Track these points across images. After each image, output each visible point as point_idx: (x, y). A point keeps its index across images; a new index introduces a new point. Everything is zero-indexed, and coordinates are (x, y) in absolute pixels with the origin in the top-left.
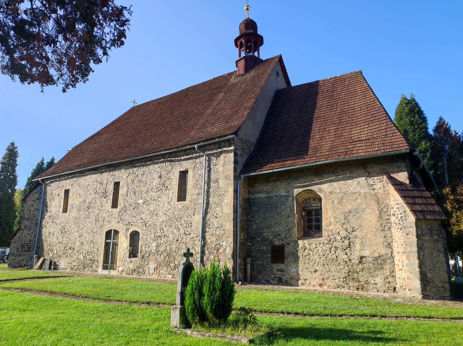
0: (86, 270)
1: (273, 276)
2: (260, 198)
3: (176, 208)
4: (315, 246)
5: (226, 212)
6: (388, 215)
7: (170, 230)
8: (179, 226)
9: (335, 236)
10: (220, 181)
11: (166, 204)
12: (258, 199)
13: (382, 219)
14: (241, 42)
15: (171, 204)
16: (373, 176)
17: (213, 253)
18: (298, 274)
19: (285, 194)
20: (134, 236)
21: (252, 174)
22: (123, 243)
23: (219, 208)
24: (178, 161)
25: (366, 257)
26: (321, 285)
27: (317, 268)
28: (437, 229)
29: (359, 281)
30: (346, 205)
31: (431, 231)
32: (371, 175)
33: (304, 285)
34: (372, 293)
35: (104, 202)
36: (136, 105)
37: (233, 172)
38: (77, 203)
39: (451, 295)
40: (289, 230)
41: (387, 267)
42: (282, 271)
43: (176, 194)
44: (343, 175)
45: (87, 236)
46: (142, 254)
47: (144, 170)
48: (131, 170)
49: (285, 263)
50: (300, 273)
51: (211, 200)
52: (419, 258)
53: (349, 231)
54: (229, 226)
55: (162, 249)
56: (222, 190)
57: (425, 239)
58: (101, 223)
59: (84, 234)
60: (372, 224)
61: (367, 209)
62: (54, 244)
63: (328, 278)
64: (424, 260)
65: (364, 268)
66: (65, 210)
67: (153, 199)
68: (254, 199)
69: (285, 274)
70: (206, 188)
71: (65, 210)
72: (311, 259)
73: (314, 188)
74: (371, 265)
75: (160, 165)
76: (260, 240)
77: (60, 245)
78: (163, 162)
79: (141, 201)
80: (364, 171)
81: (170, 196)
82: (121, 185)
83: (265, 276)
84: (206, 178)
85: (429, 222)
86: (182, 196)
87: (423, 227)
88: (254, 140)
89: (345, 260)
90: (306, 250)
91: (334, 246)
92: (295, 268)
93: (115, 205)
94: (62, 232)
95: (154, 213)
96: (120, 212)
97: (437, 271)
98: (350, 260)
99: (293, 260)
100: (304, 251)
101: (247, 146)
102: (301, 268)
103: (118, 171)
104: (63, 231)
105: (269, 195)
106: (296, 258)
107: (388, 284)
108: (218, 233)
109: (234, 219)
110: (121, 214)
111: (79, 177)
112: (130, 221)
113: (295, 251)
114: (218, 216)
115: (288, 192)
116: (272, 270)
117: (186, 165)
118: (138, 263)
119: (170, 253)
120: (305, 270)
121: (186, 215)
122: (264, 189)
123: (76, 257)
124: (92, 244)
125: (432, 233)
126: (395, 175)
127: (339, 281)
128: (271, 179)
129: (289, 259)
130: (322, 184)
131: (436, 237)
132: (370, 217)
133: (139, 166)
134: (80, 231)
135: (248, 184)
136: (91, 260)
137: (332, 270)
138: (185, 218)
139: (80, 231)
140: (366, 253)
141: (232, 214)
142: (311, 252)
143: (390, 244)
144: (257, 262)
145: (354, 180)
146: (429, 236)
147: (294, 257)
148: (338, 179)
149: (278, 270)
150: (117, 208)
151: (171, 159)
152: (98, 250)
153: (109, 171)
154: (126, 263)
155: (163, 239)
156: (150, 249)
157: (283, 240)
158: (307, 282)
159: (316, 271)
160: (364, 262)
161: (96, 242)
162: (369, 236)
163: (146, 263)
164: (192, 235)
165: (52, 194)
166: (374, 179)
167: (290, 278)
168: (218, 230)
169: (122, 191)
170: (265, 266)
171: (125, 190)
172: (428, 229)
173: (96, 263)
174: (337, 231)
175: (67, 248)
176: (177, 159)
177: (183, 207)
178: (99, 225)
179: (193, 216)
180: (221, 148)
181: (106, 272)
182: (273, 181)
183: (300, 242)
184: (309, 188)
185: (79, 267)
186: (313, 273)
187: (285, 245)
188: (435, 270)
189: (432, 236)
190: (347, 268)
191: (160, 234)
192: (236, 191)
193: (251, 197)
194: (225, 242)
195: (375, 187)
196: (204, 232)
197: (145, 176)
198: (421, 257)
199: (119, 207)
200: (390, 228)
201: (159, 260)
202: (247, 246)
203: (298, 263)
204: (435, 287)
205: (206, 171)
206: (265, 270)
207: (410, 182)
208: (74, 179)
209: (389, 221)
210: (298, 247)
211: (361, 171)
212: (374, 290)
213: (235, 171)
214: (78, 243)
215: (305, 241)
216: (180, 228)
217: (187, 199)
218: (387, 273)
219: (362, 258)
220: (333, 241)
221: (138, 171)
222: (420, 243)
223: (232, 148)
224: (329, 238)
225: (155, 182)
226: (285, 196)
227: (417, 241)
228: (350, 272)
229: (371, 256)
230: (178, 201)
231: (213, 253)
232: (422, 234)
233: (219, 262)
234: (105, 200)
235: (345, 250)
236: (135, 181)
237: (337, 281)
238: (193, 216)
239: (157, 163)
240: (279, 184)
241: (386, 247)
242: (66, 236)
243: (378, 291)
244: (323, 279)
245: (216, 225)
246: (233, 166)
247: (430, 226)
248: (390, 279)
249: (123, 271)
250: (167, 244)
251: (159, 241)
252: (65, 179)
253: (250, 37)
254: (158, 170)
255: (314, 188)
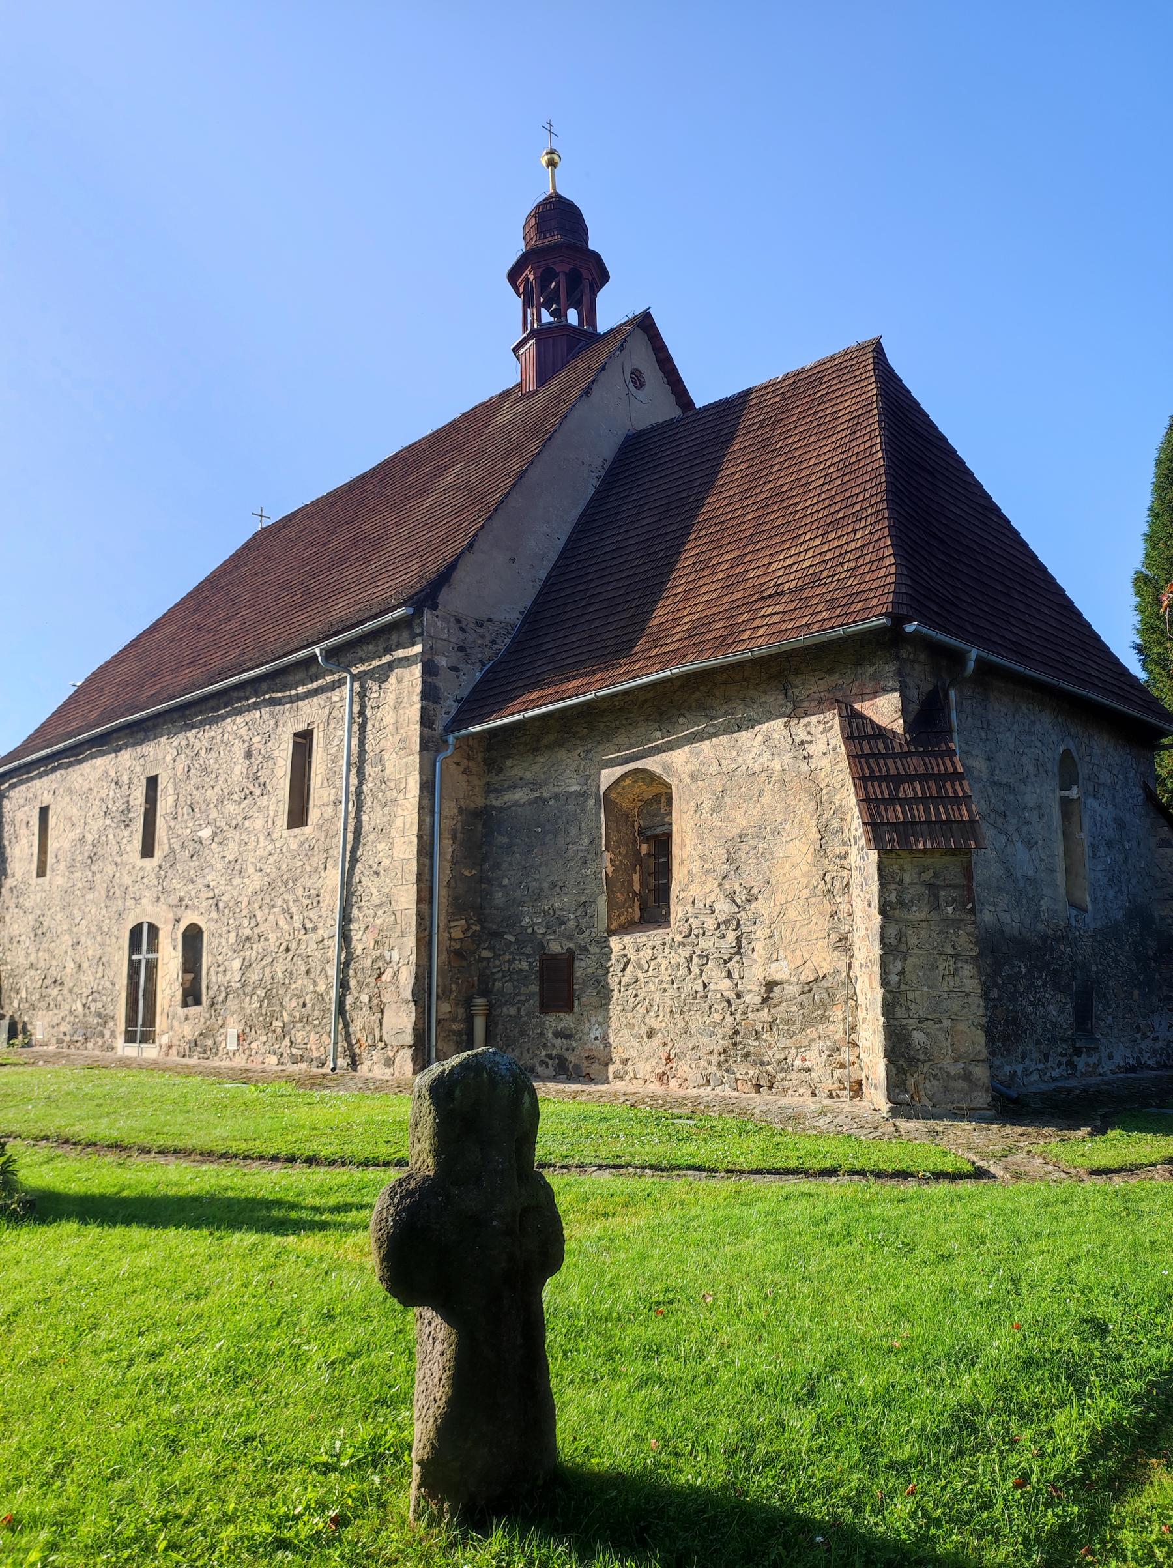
0: (90, 1045)
1: (544, 1053)
2: (516, 804)
3: (284, 850)
4: (650, 952)
5: (402, 856)
6: (845, 844)
7: (271, 917)
8: (291, 904)
9: (702, 918)
10: (386, 757)
11: (262, 839)
12: (509, 807)
13: (826, 856)
14: (527, 279)
15: (274, 836)
16: (806, 714)
17: (368, 985)
18: (607, 1045)
19: (577, 788)
20: (192, 939)
21: (476, 729)
22: (170, 960)
23: (383, 844)
24: (292, 702)
25: (782, 983)
26: (662, 1077)
27: (655, 1024)
28: (957, 881)
29: (762, 1063)
30: (733, 814)
31: (933, 889)
32: (800, 712)
33: (621, 1078)
34: (799, 1100)
35: (125, 841)
36: (267, 523)
37: (418, 727)
38: (67, 845)
39: (992, 1105)
40: (586, 905)
41: (837, 1013)
42: (566, 1035)
43: (284, 808)
44: (726, 713)
45: (89, 943)
46: (211, 993)
47: (213, 734)
48: (180, 740)
49: (576, 1010)
50: (611, 1040)
51: (365, 818)
52: (885, 983)
53: (739, 901)
54: (407, 899)
55: (253, 977)
56: (392, 785)
57: (910, 917)
58: (120, 902)
59: (83, 939)
60: (799, 874)
61: (788, 826)
62: (21, 970)
63: (682, 1055)
64: (903, 987)
65: (775, 1020)
66: (41, 873)
67: (234, 823)
68: (501, 809)
69: (574, 1044)
70: (354, 781)
71: (41, 873)
72: (641, 996)
73: (652, 764)
74: (795, 1008)
75: (248, 717)
76: (513, 939)
77: (32, 972)
78: (256, 706)
79: (205, 833)
80: (781, 700)
81: (271, 814)
82: (160, 787)
83: (525, 1054)
84: (355, 749)
85: (930, 861)
86: (298, 816)
87: (907, 879)
88: (515, 617)
89: (727, 994)
90: (630, 968)
91: (698, 952)
92: (600, 1024)
93: (148, 850)
94: (36, 935)
95: (235, 869)
96: (160, 867)
97: (947, 1023)
98: (739, 996)
99: (595, 1001)
100: (623, 970)
101: (483, 637)
102: (614, 1025)
103: (152, 744)
104: (39, 932)
105: (538, 794)
106: (604, 994)
107: (839, 1071)
108: (378, 922)
109: (420, 875)
110: (162, 873)
111: (70, 764)
112: (182, 894)
113: (600, 971)
114: (380, 869)
115: (586, 778)
116: (542, 1034)
117: (307, 712)
118: (202, 1020)
119: (271, 989)
120: (624, 1032)
121: (308, 868)
122: (528, 775)
123: (68, 1007)
124: (101, 968)
125: (937, 897)
126: (867, 704)
127: (710, 1063)
128: (545, 742)
129: (587, 997)
130: (671, 749)
131: (950, 909)
132: (794, 852)
133: (202, 724)
134: (75, 930)
135: (485, 761)
136: (99, 1015)
137: (693, 1027)
138: (305, 880)
139: (75, 930)
140: (779, 971)
141: (415, 862)
142: (641, 975)
143: (847, 939)
144: (505, 1009)
145: (757, 728)
146: (926, 909)
147: (598, 993)
148: (712, 730)
149: (557, 1035)
150: (152, 856)
151: (274, 695)
152: (113, 984)
153: (134, 745)
154: (176, 1023)
155: (255, 946)
156: (228, 978)
157: (570, 938)
158: (630, 1068)
159: (651, 1034)
160: (775, 1002)
161: (108, 962)
162: (792, 914)
163: (220, 1022)
164: (320, 931)
165: (13, 821)
166: (809, 723)
167: (588, 1058)
168: (380, 913)
169: (165, 805)
170: (526, 1023)
171: (170, 800)
172: (924, 884)
173: (111, 1024)
174: (708, 903)
175: (49, 981)
176: (288, 693)
177: (301, 844)
178: (114, 910)
179: (323, 874)
180: (388, 650)
181: (131, 1050)
182: (549, 747)
183: (615, 943)
184: (638, 765)
185: (75, 1038)
186: (646, 1040)
187: (578, 952)
188: (941, 1022)
189: (935, 906)
190: (729, 1019)
191: (248, 932)
192: (427, 787)
193: (494, 803)
194: (396, 950)
195: (811, 749)
196: (346, 919)
197: (214, 754)
198: (894, 978)
199: (158, 854)
200: (848, 884)
201: (248, 1011)
202: (481, 959)
203: (608, 1010)
204: (934, 1077)
205: (355, 728)
206: (523, 1034)
207: (908, 727)
208: (58, 773)
209: (844, 863)
210: (610, 959)
211: (774, 699)
212: (801, 1091)
213: (426, 720)
214: (70, 965)
215: (628, 940)
216: (294, 910)
217: (309, 822)
218: (837, 1031)
219: (770, 985)
220: (697, 936)
221: (199, 738)
222: (892, 930)
223: (418, 648)
224: (687, 925)
225: (238, 769)
226: (578, 794)
227: (883, 927)
228: (736, 1032)
229: (793, 979)
230: (288, 828)
231: (368, 985)
232: (901, 902)
233: (382, 1011)
234: (126, 833)
235: (726, 962)
236: (193, 771)
237: (703, 1063)
238: (323, 874)
239: (240, 712)
240: (562, 755)
241: (834, 949)
242: (45, 945)
243: (814, 1094)
244: (669, 1060)
245: (376, 900)
246: (419, 706)
247: (930, 873)
248: (845, 1055)
249: (170, 1047)
250: (264, 962)
251: (248, 953)
252: (40, 776)
253: (558, 258)
254: (243, 731)
255: (652, 764)
